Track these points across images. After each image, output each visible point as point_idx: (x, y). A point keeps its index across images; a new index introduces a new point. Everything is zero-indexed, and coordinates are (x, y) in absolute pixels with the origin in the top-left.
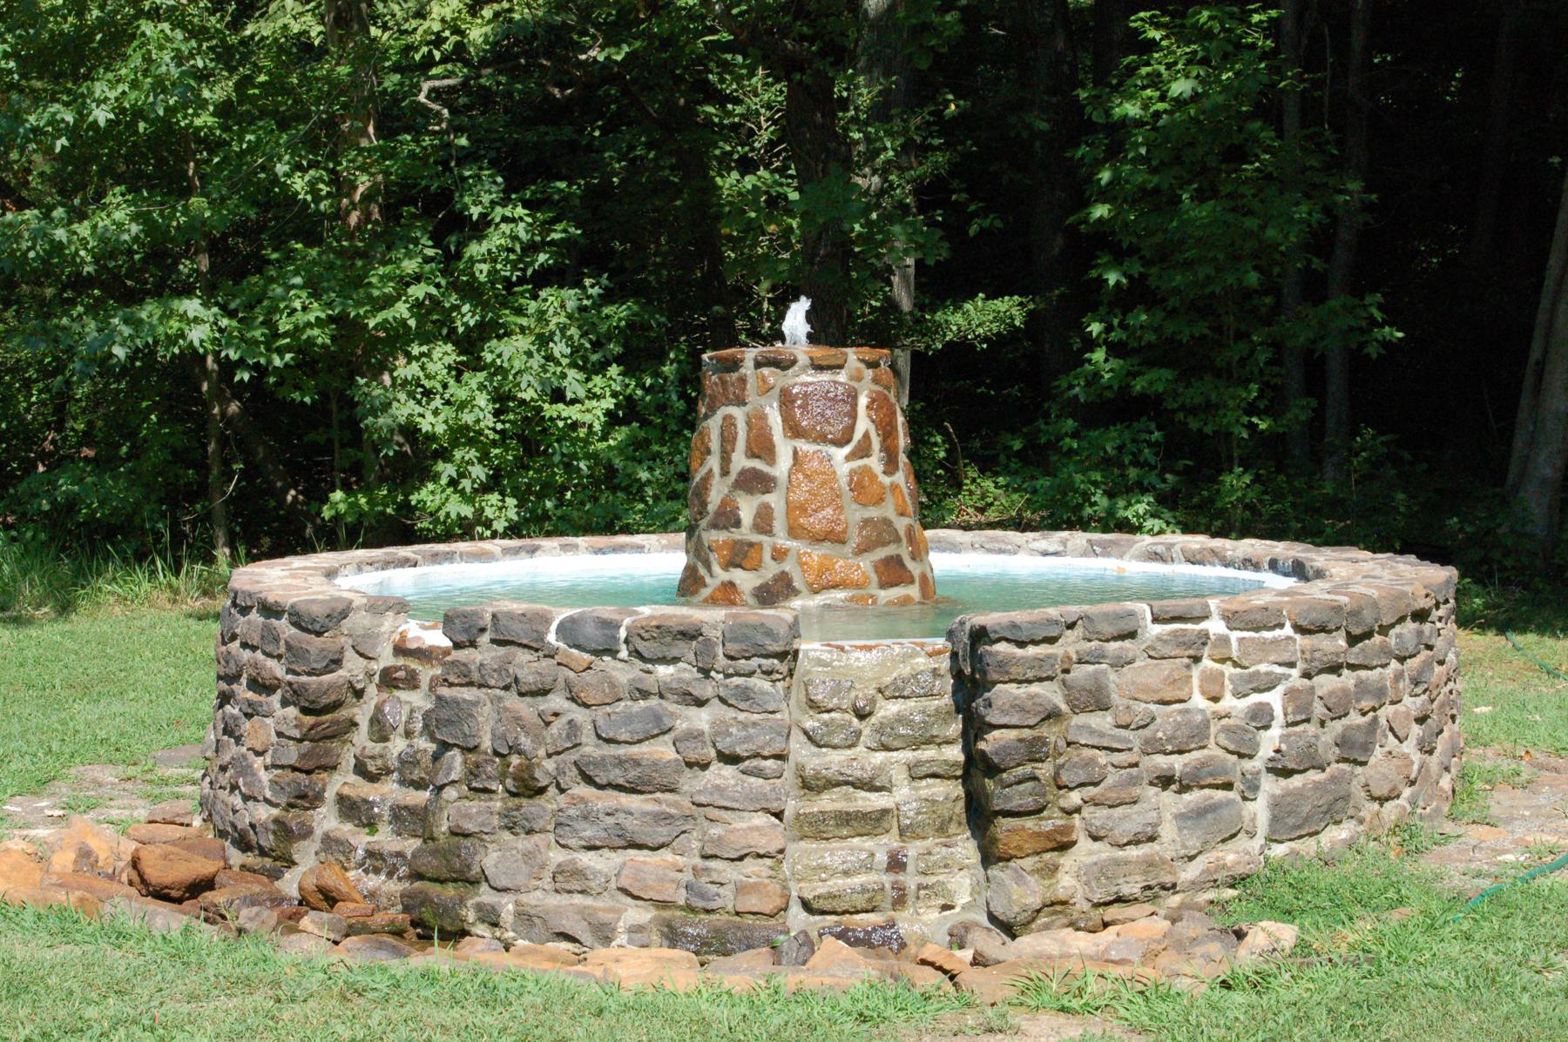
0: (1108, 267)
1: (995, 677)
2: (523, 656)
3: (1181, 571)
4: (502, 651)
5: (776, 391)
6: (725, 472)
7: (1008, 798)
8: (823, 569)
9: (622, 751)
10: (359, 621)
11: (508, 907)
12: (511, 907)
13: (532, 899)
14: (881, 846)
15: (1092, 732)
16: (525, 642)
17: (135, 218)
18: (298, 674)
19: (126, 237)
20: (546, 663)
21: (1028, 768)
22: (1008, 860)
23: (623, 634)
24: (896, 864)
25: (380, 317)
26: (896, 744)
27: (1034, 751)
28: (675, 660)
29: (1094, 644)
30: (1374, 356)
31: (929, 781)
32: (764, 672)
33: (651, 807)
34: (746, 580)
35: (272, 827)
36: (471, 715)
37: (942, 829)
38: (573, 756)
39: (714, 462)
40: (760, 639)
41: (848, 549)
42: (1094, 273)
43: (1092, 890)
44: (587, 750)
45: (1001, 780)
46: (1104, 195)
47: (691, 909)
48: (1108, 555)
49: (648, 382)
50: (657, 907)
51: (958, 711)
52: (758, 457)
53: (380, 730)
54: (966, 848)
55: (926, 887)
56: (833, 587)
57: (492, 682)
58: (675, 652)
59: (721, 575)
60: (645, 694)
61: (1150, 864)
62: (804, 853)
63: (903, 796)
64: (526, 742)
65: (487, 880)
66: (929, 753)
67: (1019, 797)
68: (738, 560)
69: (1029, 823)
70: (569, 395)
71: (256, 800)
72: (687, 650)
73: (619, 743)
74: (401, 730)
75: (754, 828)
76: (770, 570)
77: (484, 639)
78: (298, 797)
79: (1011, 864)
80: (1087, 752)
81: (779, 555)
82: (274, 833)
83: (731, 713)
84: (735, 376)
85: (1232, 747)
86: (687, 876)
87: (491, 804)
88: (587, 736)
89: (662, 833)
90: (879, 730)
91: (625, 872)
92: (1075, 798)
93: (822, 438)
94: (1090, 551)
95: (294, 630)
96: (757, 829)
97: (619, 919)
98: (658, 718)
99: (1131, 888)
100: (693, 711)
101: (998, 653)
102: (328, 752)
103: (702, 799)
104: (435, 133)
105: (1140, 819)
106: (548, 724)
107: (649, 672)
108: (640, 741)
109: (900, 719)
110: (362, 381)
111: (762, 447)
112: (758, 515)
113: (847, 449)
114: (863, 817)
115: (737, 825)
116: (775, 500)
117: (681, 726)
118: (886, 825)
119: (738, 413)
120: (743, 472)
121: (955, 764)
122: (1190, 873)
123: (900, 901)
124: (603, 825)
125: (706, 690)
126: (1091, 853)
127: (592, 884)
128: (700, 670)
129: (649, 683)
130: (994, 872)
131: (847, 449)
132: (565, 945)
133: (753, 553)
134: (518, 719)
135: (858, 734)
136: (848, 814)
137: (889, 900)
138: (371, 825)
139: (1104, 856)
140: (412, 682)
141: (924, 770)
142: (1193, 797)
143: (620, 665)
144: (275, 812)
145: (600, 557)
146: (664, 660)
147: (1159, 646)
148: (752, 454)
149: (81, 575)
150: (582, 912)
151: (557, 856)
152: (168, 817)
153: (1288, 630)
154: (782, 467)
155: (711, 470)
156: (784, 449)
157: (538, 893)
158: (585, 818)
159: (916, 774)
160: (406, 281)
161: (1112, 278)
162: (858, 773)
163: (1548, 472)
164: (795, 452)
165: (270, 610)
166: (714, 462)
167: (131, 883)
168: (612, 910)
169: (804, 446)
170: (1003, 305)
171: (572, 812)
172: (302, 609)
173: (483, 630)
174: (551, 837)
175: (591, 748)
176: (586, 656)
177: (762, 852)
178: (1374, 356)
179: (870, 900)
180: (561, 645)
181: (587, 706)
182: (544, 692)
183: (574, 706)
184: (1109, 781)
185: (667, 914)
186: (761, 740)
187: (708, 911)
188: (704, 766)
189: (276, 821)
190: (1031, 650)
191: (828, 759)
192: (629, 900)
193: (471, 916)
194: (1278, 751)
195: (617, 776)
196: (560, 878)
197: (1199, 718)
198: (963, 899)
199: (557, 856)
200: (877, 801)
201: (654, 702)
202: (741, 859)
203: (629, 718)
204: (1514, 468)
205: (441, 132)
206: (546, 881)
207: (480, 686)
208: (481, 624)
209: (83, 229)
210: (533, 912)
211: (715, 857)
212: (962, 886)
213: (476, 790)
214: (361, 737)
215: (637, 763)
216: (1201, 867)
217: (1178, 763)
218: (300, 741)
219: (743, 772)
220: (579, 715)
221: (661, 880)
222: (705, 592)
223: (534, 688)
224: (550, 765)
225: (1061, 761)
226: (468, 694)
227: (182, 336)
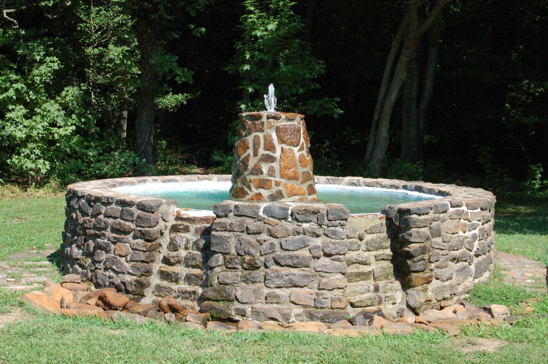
0: (248, 85)
1: (413, 226)
3: (362, 189)
4: (239, 219)
5: (275, 127)
6: (255, 155)
7: (416, 267)
8: (292, 189)
9: (291, 253)
11: (249, 309)
12: (250, 309)
13: (258, 306)
14: (370, 283)
15: (438, 244)
16: (250, 215)
18: (144, 227)
20: (259, 223)
21: (421, 256)
22: (414, 287)
23: (290, 212)
24: (377, 289)
26: (372, 249)
27: (424, 250)
28: (310, 221)
29: (438, 214)
30: (336, 118)
31: (382, 261)
32: (341, 225)
33: (301, 273)
34: (265, 193)
35: (134, 283)
36: (227, 242)
37: (386, 278)
39: (250, 151)
40: (341, 214)
41: (299, 182)
43: (438, 296)
44: (278, 253)
45: (414, 261)
46: (248, 62)
47: (317, 308)
48: (335, 183)
50: (304, 307)
51: (389, 238)
52: (269, 150)
53: (173, 247)
54: (397, 284)
55: (388, 297)
56: (295, 195)
57: (236, 230)
58: (309, 219)
59: (255, 191)
60: (298, 233)
61: (452, 287)
63: (374, 266)
64: (252, 251)
65: (237, 300)
66: (381, 252)
68: (262, 186)
69: (421, 274)
70: (58, 125)
71: (123, 273)
72: (314, 218)
73: (289, 250)
74: (183, 247)
75: (337, 279)
76: (274, 189)
77: (231, 214)
78: (146, 272)
79: (415, 288)
80: (437, 251)
81: (277, 184)
82: (135, 285)
83: (329, 240)
84: (259, 122)
85: (469, 248)
86: (315, 296)
87: (237, 273)
89: (305, 281)
90: (367, 244)
91: (292, 296)
92: (433, 266)
93: (291, 144)
94: (328, 182)
96: (339, 279)
97: (291, 312)
98: (304, 242)
99: (447, 295)
100: (315, 239)
101: (414, 218)
102: (153, 255)
104: (14, 29)
105: (449, 272)
106: (261, 244)
107: (300, 226)
108: (297, 250)
109: (372, 240)
111: (270, 147)
112: (269, 170)
114: (363, 274)
116: (276, 165)
117: (312, 244)
118: (370, 276)
119: (260, 135)
120: (263, 155)
121: (390, 255)
122: (460, 289)
123: (380, 303)
124: (284, 279)
125: (320, 231)
126: (436, 284)
127: (282, 300)
129: (300, 230)
130: (410, 291)
132: (272, 322)
133: (268, 183)
134: (249, 243)
135: (359, 246)
136: (360, 273)
137: (377, 302)
138: (177, 281)
139: (440, 284)
141: (380, 257)
142: (460, 264)
143: (288, 223)
144: (135, 278)
145: (164, 183)
146: (306, 222)
147: (453, 215)
150: (279, 310)
151: (266, 291)
152: (72, 280)
153: (479, 210)
154: (278, 154)
155: (249, 154)
157: (259, 304)
158: (277, 277)
162: (361, 259)
163: (380, 156)
164: (282, 149)
165: (123, 203)
166: (250, 151)
167: (98, 305)
168: (288, 309)
169: (284, 146)
170: (180, 97)
171: (273, 275)
173: (231, 211)
174: (263, 284)
175: (279, 252)
176: (276, 220)
177: (340, 287)
178: (336, 118)
179: (372, 302)
180: (265, 216)
181: (277, 238)
182: (259, 233)
183: (271, 238)
184: (441, 260)
185: (308, 309)
186: (340, 248)
187: (322, 308)
188: (318, 258)
189: (136, 281)
190: (423, 217)
191: (351, 255)
192: (293, 305)
193: (233, 313)
194: (478, 249)
195: (289, 262)
196: (268, 298)
197: (462, 238)
198: (399, 300)
199: (266, 291)
200: (366, 269)
201: (302, 236)
202: (333, 290)
203: (294, 242)
204: (368, 155)
205: (16, 29)
206: (263, 300)
207: (230, 231)
208: (231, 209)
210: (260, 311)
211: (324, 289)
212: (399, 296)
213: (229, 268)
214: (164, 251)
215: (298, 257)
216: (463, 287)
218: (145, 252)
219: (332, 260)
220: (276, 241)
221: (305, 298)
222: (248, 197)
223: (255, 232)
224: (262, 259)
225: (431, 254)
226: (226, 234)
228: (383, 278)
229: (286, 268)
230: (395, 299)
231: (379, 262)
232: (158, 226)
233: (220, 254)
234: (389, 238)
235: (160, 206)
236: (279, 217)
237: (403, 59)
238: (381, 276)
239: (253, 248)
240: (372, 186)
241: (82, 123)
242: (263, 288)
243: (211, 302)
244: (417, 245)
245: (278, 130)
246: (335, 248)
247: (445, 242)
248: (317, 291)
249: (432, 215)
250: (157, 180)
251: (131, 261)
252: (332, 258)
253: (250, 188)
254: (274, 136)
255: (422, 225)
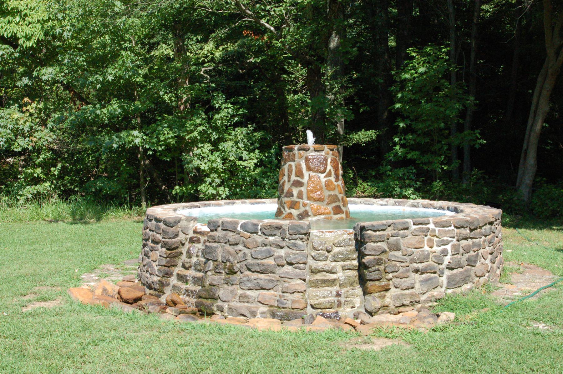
0: (400, 122)
1: (367, 240)
2: (231, 234)
4: (224, 232)
5: (304, 157)
6: (289, 181)
9: (259, 261)
10: (183, 223)
11: (226, 306)
12: (227, 306)
13: (233, 304)
17: (119, 107)
19: (117, 113)
20: (237, 236)
23: (259, 227)
24: (338, 295)
25: (189, 136)
26: (338, 260)
27: (379, 262)
28: (274, 235)
29: (396, 231)
33: (267, 278)
34: (295, 212)
37: (352, 285)
38: (245, 263)
39: (286, 178)
40: (299, 229)
42: (396, 124)
44: (249, 261)
46: (399, 101)
47: (279, 307)
49: (267, 155)
51: (356, 250)
54: (359, 290)
57: (222, 241)
58: (274, 233)
59: (288, 211)
60: (266, 245)
61: (412, 295)
62: (312, 291)
63: (340, 275)
64: (231, 259)
66: (348, 262)
67: (374, 275)
69: (377, 283)
72: (278, 232)
75: (297, 284)
76: (302, 209)
77: (219, 229)
81: (305, 205)
83: (290, 251)
85: (436, 261)
86: (278, 298)
88: (249, 257)
89: (271, 285)
90: (334, 256)
91: (260, 297)
92: (390, 276)
93: (318, 171)
94: (395, 204)
95: (165, 226)
96: (298, 284)
98: (269, 252)
99: (407, 302)
100: (280, 250)
103: (282, 275)
104: (205, 83)
106: (238, 253)
109: (340, 253)
110: (184, 154)
111: (300, 174)
113: (325, 174)
114: (329, 281)
115: (292, 283)
116: (303, 189)
117: (276, 254)
118: (335, 283)
119: (293, 164)
120: (294, 181)
121: (356, 266)
122: (424, 298)
123: (339, 305)
125: (284, 244)
126: (395, 292)
128: (282, 238)
129: (267, 242)
130: (367, 297)
131: (325, 174)
132: (242, 317)
133: (297, 204)
135: (327, 257)
138: (186, 282)
139: (399, 293)
140: (198, 241)
144: (159, 278)
146: (271, 235)
147: (415, 232)
148: (297, 176)
149: (103, 210)
150: (248, 308)
151: (240, 292)
153: (452, 227)
154: (305, 180)
156: (306, 174)
157: (235, 302)
159: (344, 269)
160: (197, 125)
161: (401, 125)
162: (327, 268)
163: (528, 182)
164: (309, 175)
165: (158, 220)
166: (286, 178)
167: (118, 298)
168: (256, 307)
169: (312, 174)
172: (167, 220)
173: (219, 226)
174: (239, 286)
175: (250, 261)
180: (242, 231)
182: (237, 244)
184: (400, 271)
185: (272, 309)
187: (284, 308)
188: (283, 266)
189: (159, 281)
190: (378, 233)
193: (215, 309)
196: (241, 298)
197: (427, 253)
198: (358, 305)
199: (240, 292)
200: (333, 276)
201: (268, 247)
202: (293, 293)
203: (261, 252)
205: (207, 82)
207: (218, 242)
208: (219, 224)
209: (105, 110)
211: (286, 292)
212: (357, 301)
214: (184, 257)
215: (263, 265)
217: (420, 266)
218: (166, 258)
222: (283, 216)
224: (238, 265)
225: (386, 265)
226: (214, 245)
227: (133, 141)
228: (348, 285)
229: (255, 273)
230: (354, 303)
231: (344, 272)
232: (178, 238)
233: (211, 261)
234: (356, 250)
235: (179, 222)
236: (251, 231)
237: (545, 93)
238: (346, 283)
239: (232, 256)
240: (427, 208)
241: (266, 157)
242: (238, 289)
243: (203, 300)
244: (372, 257)
245: (307, 160)
246: (295, 258)
247: (405, 255)
248: (281, 293)
249: (389, 231)
250: (246, 202)
251: (159, 265)
252: (294, 266)
253: (284, 208)
254: (304, 166)
255: (377, 240)
